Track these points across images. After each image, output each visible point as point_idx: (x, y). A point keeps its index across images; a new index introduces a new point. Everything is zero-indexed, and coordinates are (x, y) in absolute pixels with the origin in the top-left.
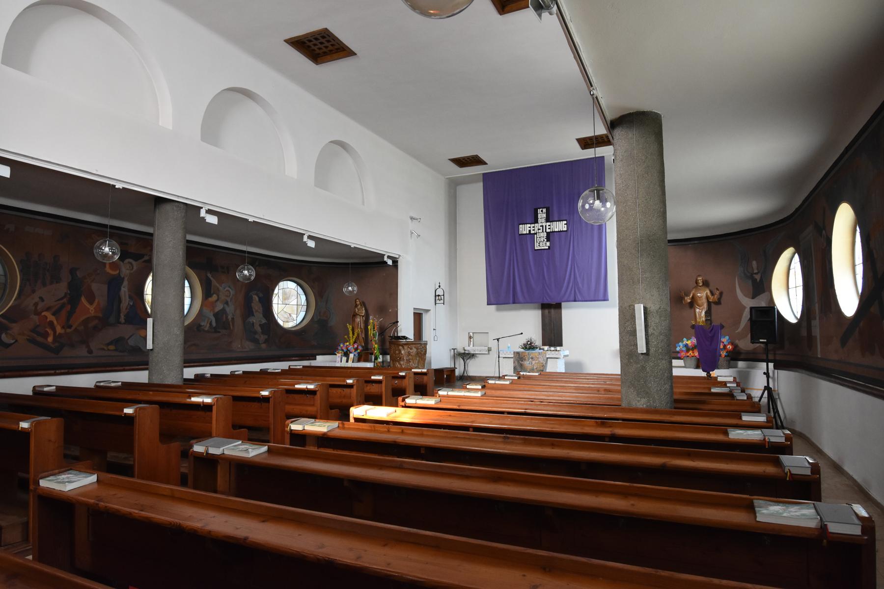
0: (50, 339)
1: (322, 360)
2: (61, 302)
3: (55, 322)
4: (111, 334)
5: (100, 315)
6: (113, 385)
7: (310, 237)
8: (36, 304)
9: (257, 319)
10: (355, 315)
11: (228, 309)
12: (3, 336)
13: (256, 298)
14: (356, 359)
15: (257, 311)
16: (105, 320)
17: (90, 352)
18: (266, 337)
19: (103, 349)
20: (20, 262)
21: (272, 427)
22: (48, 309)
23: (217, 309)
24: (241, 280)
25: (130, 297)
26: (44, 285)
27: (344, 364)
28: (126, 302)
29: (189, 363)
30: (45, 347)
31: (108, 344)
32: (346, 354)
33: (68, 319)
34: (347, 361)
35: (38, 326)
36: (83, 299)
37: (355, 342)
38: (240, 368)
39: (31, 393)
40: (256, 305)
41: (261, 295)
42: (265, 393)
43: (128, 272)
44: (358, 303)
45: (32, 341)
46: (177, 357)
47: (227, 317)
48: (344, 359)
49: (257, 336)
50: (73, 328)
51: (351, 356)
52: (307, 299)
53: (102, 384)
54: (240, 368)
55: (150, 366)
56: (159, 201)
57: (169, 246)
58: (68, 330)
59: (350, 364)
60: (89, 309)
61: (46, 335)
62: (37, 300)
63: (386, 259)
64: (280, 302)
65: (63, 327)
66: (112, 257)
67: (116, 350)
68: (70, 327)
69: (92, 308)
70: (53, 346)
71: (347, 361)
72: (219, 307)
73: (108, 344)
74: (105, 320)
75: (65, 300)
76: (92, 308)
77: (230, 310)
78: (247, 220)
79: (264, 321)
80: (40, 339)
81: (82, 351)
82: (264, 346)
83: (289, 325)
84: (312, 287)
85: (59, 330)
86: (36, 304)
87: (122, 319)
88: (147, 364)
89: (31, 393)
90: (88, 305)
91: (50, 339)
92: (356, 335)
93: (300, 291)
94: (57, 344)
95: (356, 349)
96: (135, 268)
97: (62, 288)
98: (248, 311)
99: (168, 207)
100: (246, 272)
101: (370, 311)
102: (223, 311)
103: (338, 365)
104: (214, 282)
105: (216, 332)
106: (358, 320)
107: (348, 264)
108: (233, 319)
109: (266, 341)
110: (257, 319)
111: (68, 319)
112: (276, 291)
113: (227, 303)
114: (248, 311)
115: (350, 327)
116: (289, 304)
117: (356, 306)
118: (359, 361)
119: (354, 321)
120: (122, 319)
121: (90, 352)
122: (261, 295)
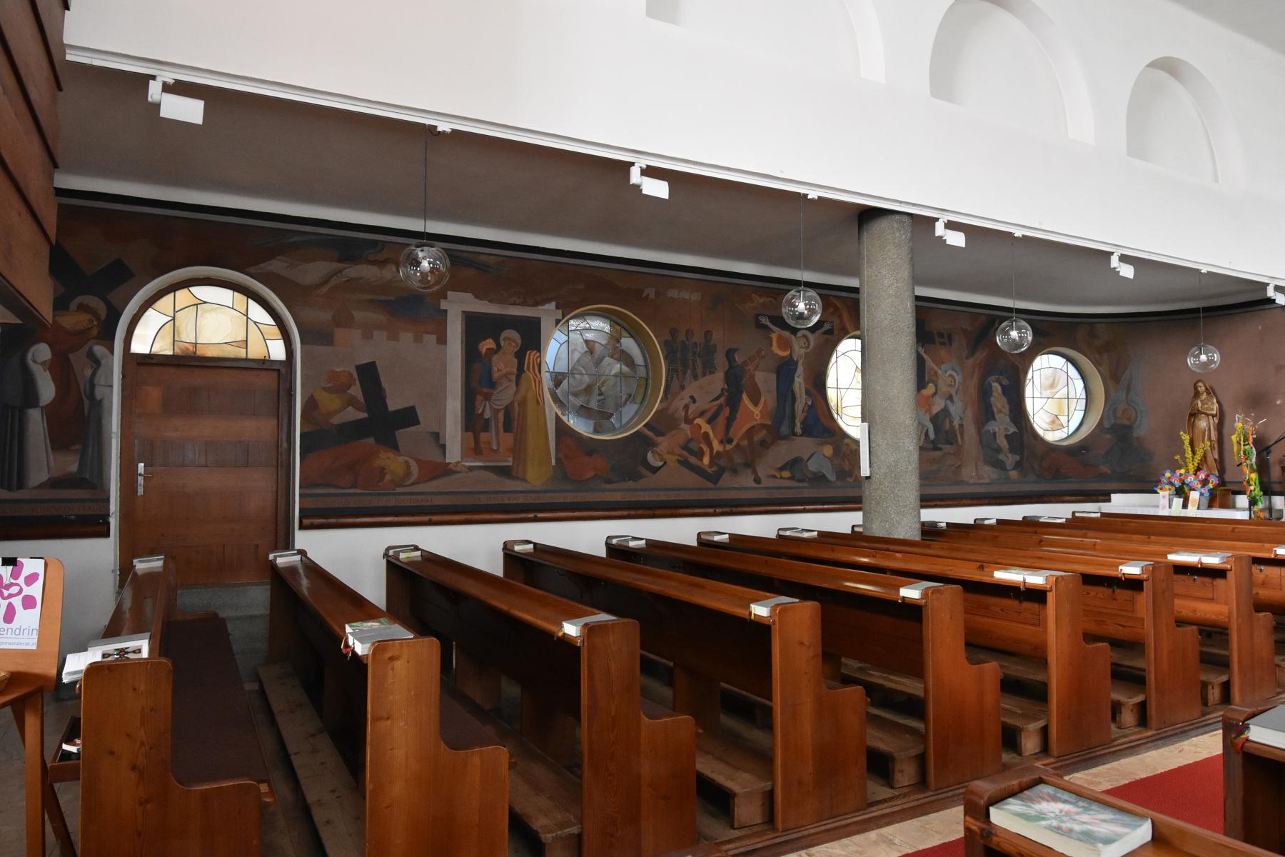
0: (706, 460)
1: (1121, 503)
2: (717, 402)
3: (711, 433)
4: (782, 452)
5: (769, 423)
6: (806, 535)
7: (1124, 259)
8: (686, 407)
9: (1002, 425)
10: (1194, 414)
11: (952, 409)
12: (650, 456)
13: (997, 387)
14: (1205, 502)
15: (1000, 411)
16: (776, 430)
17: (757, 481)
18: (1017, 458)
19: (774, 476)
20: (666, 345)
21: (1151, 642)
22: (702, 414)
23: (936, 409)
24: (1005, 348)
25: (807, 392)
26: (695, 377)
27: (1176, 509)
28: (802, 401)
29: (928, 501)
30: (699, 471)
31: (782, 469)
32: (1182, 492)
33: (728, 427)
34: (1185, 506)
35: (690, 440)
36: (745, 398)
37: (1198, 469)
38: (992, 514)
39: (695, 544)
40: (999, 402)
41: (1005, 382)
42: (1132, 569)
43: (803, 351)
44: (1201, 389)
45: (684, 463)
46: (911, 494)
47: (951, 422)
48: (1178, 502)
49: (1001, 457)
50: (734, 443)
51: (1194, 496)
52: (1086, 387)
53: (788, 533)
54: (992, 514)
55: (866, 504)
56: (867, 215)
57: (889, 292)
58: (729, 447)
59: (1192, 511)
60: (754, 413)
61: (700, 455)
62: (687, 400)
63: (1271, 293)
64: (1037, 394)
65: (721, 442)
66: (808, 318)
67: (792, 478)
68: (730, 441)
69: (757, 411)
70: (709, 470)
71: (1185, 506)
72: (939, 405)
73: (782, 469)
74: (776, 430)
75: (722, 400)
76: (757, 411)
77: (956, 409)
78: (1010, 235)
79: (1012, 429)
80: (693, 460)
81: (746, 480)
82: (1014, 474)
83: (1051, 437)
84: (1097, 364)
85: (717, 446)
86: (686, 407)
87: (798, 430)
88: (860, 502)
89: (695, 544)
90: (751, 407)
91: (706, 460)
92: (1199, 454)
93: (1073, 372)
94: (715, 468)
95: (1204, 483)
96: (812, 343)
97: (716, 382)
98: (985, 413)
99: (882, 224)
100: (1014, 334)
101: (1225, 408)
102: (945, 411)
103: (1165, 512)
104: (929, 363)
105: (936, 449)
106: (1202, 423)
107: (1196, 310)
108: (961, 426)
109: (1018, 465)
110: (1002, 425)
111: (728, 427)
112: (1029, 376)
113: (950, 398)
114: (985, 413)
115: (1186, 438)
116: (1056, 397)
117: (1197, 394)
118: (1210, 506)
119: (1192, 426)
120: (798, 430)
121: (757, 481)
122: (1005, 382)
